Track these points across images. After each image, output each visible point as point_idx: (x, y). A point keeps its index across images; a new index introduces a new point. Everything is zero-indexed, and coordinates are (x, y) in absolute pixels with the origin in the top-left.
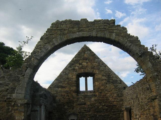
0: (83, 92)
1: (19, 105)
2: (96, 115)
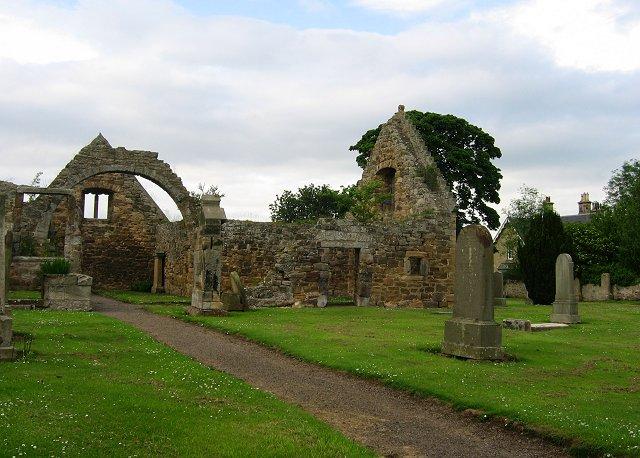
0: (90, 221)
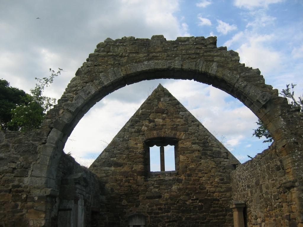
0: (156, 174)
1: (36, 198)
2: (180, 217)
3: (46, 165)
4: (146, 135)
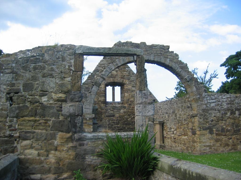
0: (111, 103)
1: (88, 119)
2: (125, 127)
3: (92, 103)
4: (106, 80)
